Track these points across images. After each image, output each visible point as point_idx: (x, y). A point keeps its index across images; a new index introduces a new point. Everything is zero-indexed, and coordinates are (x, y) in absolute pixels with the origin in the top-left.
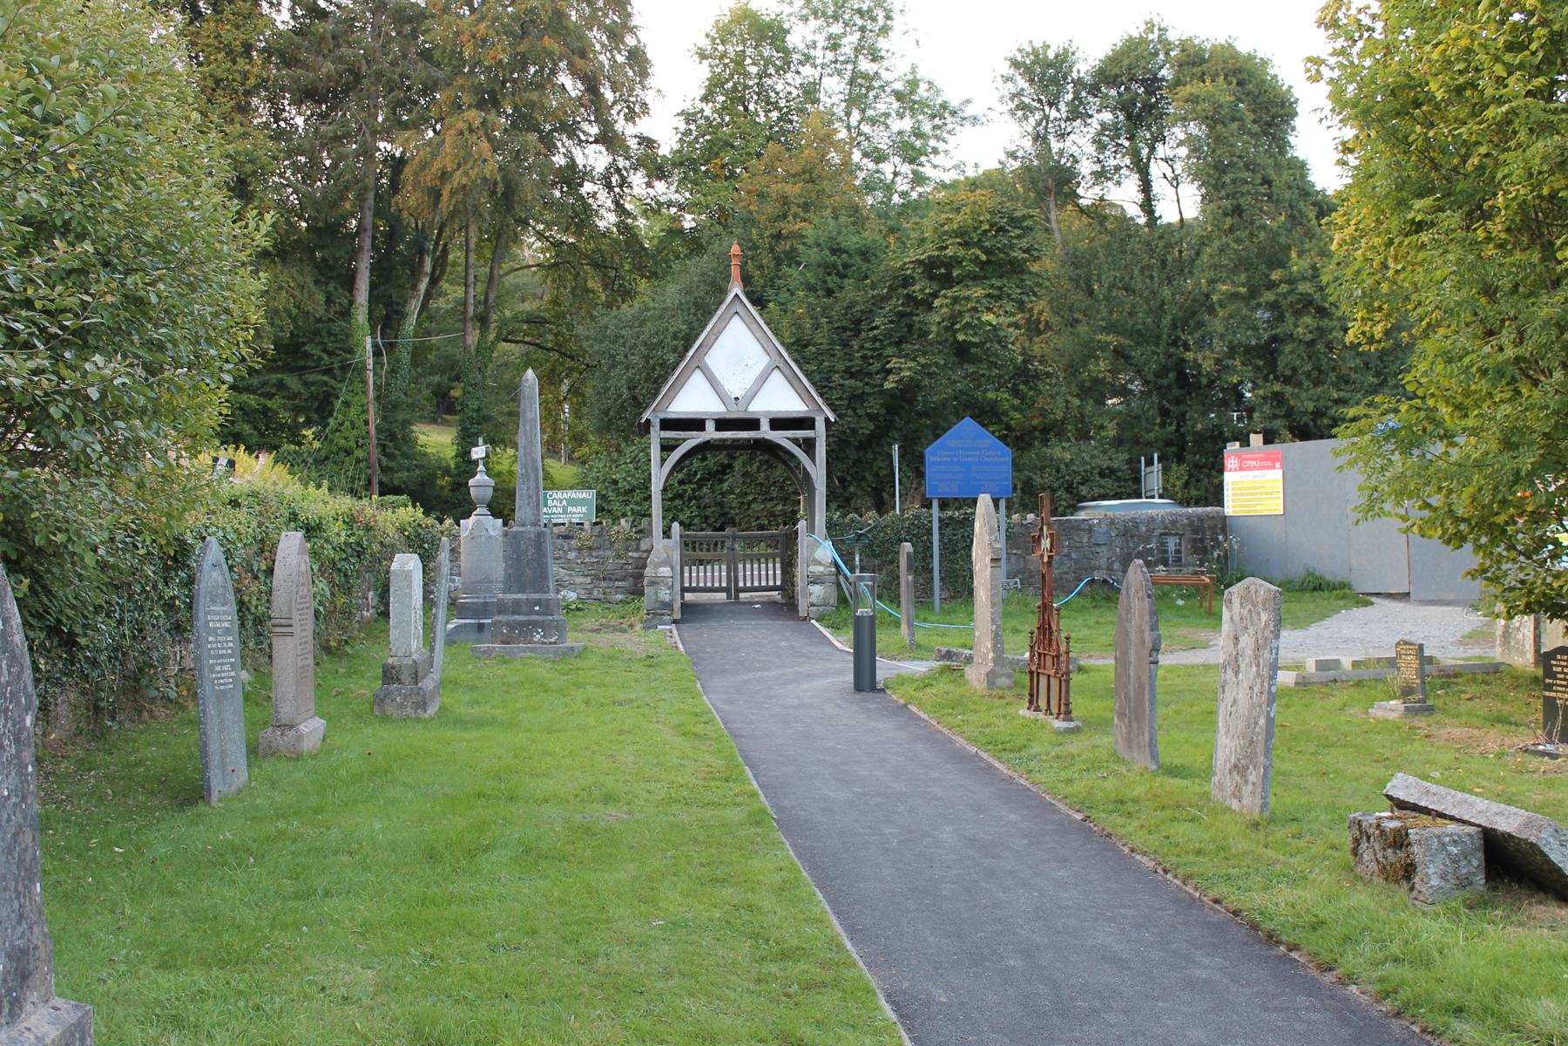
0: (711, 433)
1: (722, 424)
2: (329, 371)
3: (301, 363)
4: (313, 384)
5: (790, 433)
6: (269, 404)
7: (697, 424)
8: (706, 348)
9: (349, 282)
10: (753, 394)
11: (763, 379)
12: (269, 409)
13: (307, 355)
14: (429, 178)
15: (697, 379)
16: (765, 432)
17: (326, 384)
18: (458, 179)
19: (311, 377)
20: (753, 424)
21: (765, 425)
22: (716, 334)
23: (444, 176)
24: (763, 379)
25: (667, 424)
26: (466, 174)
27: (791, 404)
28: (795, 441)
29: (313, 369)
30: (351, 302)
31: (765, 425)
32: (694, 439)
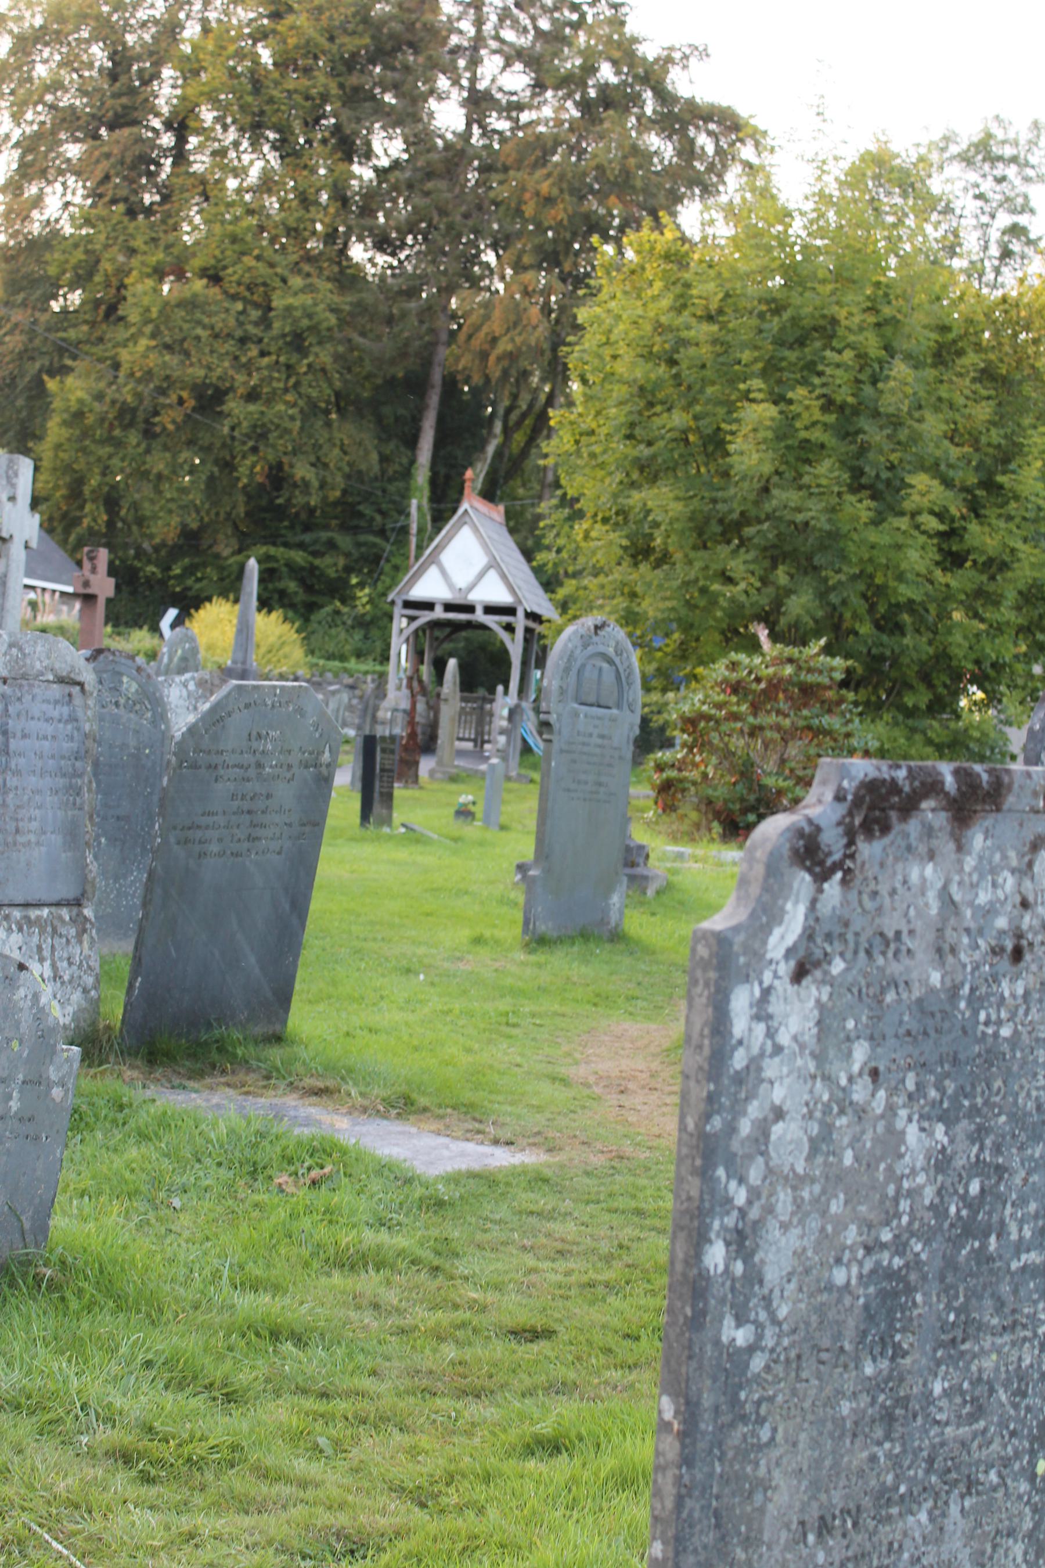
0: (439, 613)
1: (449, 607)
2: (382, 533)
3: (355, 522)
4: (365, 544)
5: (497, 618)
6: (317, 562)
7: (429, 606)
8: (440, 548)
9: (412, 442)
10: (472, 587)
11: (481, 575)
12: (317, 568)
13: (361, 515)
14: (476, 343)
15: (433, 572)
16: (479, 616)
17: (374, 545)
18: (504, 346)
19: (362, 538)
20: (470, 609)
21: (479, 611)
22: (449, 538)
23: (494, 341)
24: (481, 575)
25: (408, 604)
26: (512, 340)
27: (502, 596)
28: (499, 623)
29: (370, 530)
30: (413, 462)
31: (479, 611)
32: (426, 617)
